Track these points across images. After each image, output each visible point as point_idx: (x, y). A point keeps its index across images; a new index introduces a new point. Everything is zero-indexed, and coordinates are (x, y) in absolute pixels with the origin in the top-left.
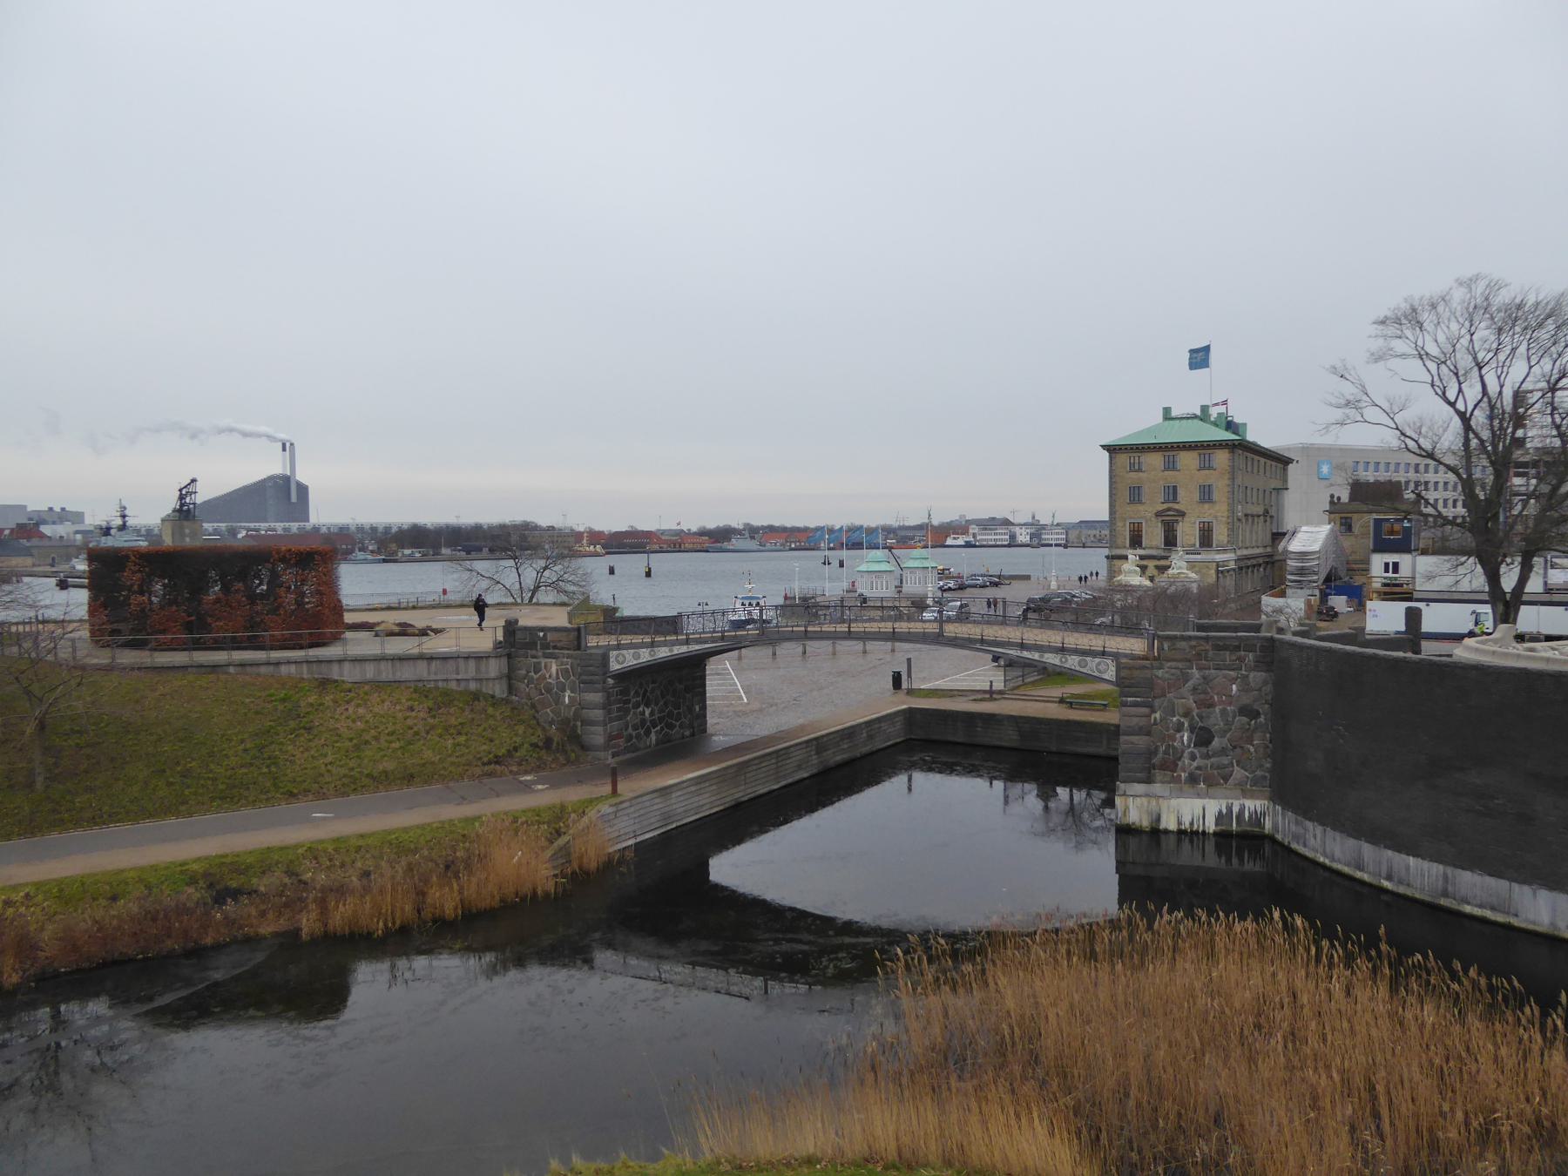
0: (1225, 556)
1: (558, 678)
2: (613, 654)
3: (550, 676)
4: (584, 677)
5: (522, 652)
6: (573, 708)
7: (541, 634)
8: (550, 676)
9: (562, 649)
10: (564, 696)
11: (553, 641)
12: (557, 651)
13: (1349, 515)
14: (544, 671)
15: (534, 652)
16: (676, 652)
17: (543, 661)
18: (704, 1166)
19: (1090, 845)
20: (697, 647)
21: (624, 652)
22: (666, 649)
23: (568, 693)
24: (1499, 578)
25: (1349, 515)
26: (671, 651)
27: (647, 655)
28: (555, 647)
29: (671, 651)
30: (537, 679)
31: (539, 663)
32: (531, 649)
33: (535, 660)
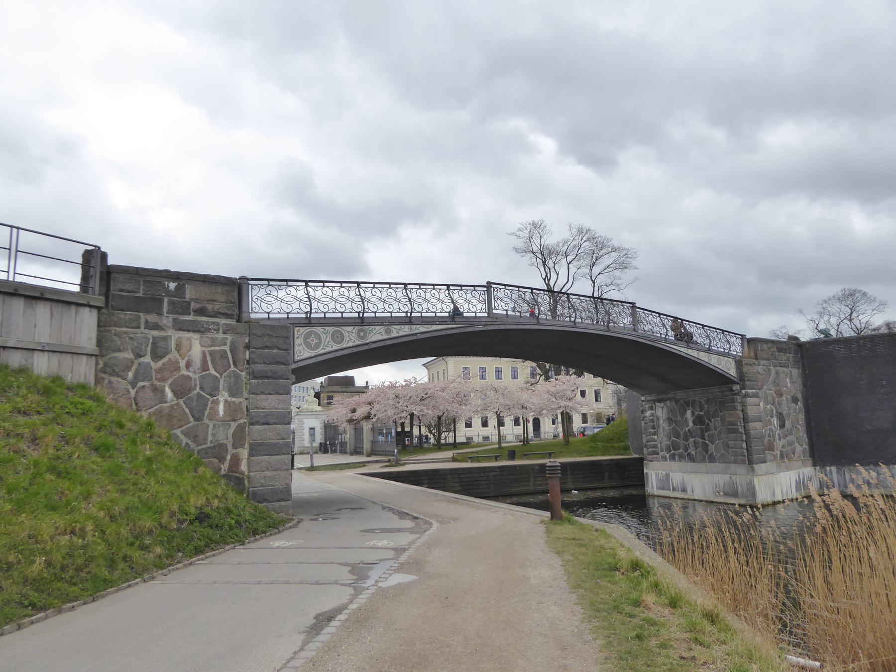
0: (127, 329)
1: (205, 367)
2: (300, 332)
3: (188, 365)
4: (259, 367)
5: (127, 315)
6: (234, 425)
7: (172, 285)
8: (188, 365)
9: (217, 314)
10: (217, 403)
11: (196, 300)
12: (204, 319)
13: (332, 394)
14: (173, 355)
15: (152, 318)
16: (394, 334)
17: (175, 336)
18: (501, 415)
19: (567, 522)
20: (423, 329)
21: (319, 330)
22: (381, 329)
23: (223, 397)
24: (603, 377)
25: (332, 394)
26: (388, 332)
27: (354, 336)
28: (201, 312)
29: (388, 332)
30: (159, 371)
31: (166, 339)
32: (148, 312)
33: (155, 333)
